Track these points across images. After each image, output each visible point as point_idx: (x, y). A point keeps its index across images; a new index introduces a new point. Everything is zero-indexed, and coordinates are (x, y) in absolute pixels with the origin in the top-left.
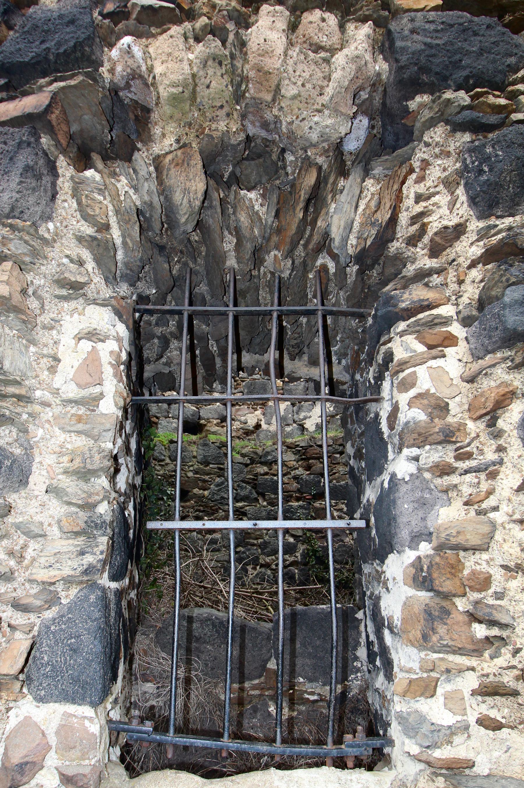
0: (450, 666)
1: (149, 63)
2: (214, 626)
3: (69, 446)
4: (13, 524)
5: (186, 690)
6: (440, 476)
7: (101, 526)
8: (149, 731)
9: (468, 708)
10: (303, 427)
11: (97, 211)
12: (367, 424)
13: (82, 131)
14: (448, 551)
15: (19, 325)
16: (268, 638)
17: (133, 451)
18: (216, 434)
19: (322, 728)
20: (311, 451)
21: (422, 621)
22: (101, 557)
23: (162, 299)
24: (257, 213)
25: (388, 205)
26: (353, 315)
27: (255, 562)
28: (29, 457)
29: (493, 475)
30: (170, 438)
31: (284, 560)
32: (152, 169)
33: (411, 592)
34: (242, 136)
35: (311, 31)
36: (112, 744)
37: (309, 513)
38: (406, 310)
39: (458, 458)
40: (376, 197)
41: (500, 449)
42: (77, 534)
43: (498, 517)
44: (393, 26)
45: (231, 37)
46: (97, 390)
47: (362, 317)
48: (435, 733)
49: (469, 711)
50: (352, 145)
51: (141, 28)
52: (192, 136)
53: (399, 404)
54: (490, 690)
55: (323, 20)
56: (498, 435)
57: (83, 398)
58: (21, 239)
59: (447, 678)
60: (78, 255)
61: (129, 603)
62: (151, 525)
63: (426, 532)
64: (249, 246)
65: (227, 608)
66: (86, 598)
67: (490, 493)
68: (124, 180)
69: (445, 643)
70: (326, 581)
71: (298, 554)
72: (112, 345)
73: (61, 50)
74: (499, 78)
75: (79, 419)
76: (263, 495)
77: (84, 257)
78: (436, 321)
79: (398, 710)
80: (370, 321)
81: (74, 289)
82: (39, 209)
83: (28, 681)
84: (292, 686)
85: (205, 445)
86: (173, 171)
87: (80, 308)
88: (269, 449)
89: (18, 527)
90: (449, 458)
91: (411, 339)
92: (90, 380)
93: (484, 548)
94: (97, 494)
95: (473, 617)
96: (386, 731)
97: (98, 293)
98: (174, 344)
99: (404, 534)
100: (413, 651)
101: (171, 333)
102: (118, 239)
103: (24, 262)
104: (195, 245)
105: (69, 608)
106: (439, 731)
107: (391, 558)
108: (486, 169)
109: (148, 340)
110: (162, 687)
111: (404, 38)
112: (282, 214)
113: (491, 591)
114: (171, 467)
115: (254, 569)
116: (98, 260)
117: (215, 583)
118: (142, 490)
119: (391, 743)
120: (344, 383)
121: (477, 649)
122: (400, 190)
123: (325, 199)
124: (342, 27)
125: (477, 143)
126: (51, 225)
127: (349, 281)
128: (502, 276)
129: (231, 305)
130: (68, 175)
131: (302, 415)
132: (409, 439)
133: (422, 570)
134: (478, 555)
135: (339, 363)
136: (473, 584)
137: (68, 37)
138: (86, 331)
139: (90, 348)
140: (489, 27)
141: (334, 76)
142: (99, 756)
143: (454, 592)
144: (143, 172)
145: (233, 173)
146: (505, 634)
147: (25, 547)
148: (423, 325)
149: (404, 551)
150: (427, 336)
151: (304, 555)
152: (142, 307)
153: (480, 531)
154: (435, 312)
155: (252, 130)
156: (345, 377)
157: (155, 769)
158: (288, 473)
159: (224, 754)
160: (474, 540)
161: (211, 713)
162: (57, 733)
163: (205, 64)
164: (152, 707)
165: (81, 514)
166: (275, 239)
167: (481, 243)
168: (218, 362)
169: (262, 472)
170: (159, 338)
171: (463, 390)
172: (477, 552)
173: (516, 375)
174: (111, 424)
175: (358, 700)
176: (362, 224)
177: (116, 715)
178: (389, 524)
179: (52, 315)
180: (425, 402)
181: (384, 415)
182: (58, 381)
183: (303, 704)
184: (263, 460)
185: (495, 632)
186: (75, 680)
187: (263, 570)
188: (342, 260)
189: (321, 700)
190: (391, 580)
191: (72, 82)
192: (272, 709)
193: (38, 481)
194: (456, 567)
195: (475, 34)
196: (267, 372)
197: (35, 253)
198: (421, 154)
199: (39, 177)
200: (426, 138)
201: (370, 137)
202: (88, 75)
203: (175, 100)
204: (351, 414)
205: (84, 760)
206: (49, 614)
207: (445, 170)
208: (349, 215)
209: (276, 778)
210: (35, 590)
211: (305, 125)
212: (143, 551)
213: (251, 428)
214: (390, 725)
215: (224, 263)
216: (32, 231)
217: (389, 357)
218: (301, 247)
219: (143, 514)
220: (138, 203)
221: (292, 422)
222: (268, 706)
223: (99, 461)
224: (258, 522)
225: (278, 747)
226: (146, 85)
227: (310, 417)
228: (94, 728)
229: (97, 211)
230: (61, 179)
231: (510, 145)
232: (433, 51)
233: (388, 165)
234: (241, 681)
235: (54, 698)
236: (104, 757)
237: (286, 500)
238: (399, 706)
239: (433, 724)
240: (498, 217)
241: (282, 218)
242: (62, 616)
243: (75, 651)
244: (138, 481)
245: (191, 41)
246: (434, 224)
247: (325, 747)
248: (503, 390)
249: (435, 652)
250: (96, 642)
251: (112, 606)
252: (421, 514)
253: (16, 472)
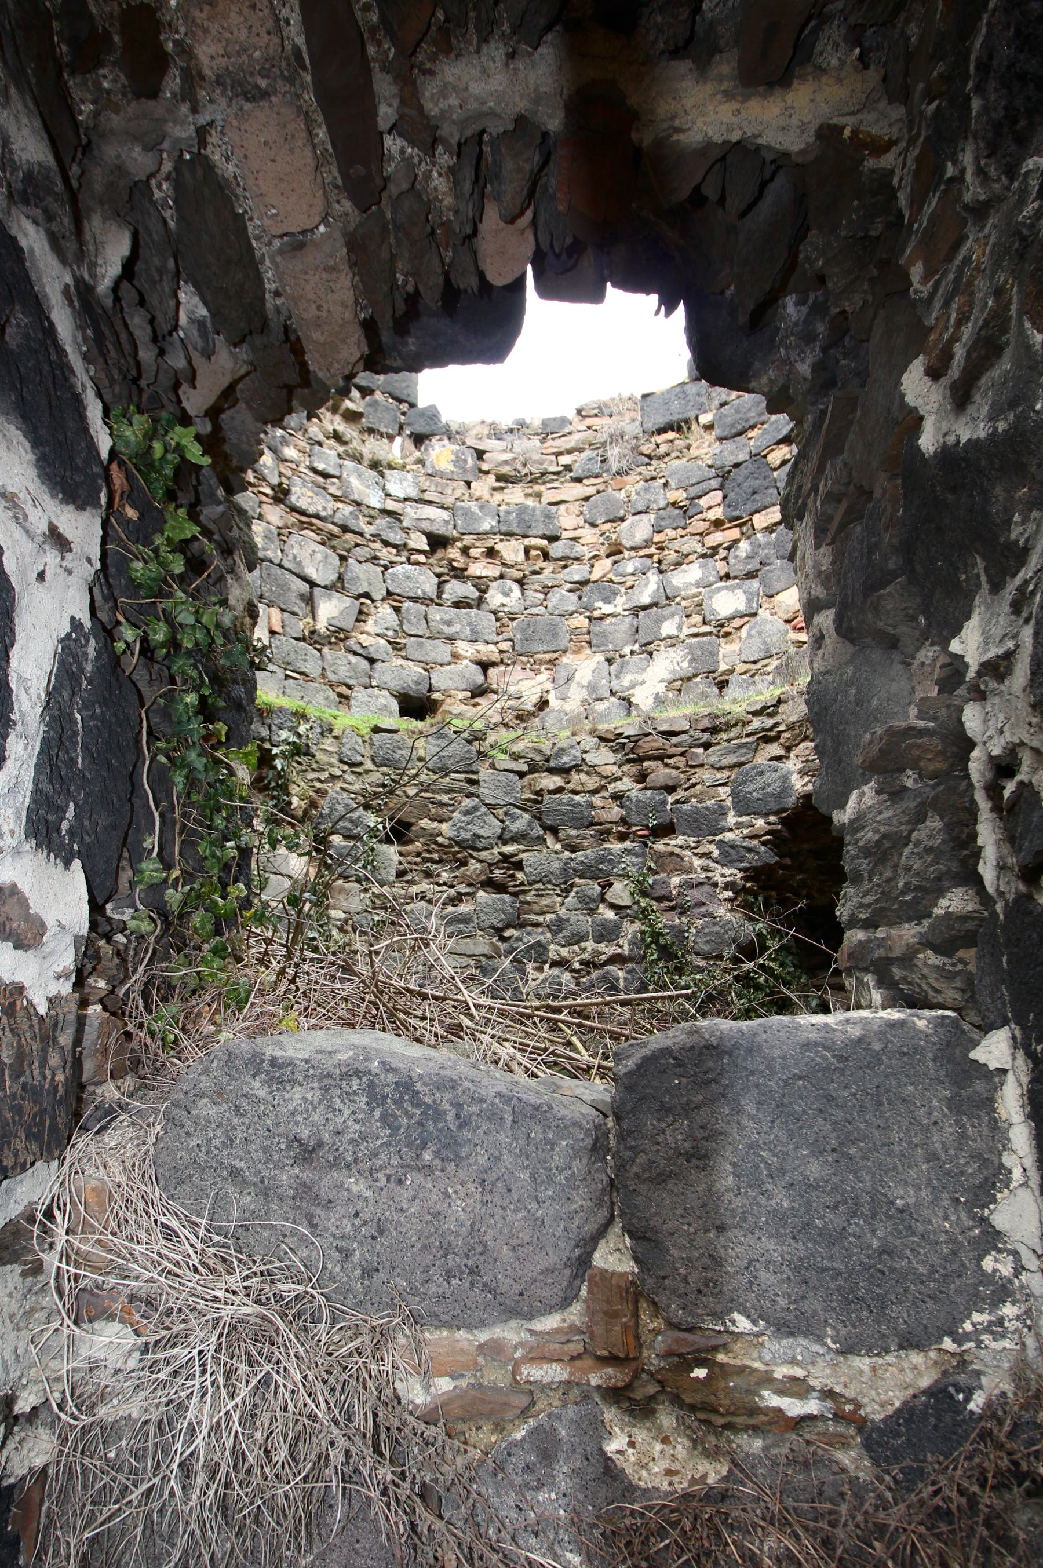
2: (375, 1097)
10: (630, 703)
30: (373, 723)
37: (644, 863)
76: (554, 831)
88: (564, 744)
115: (540, 969)
120: (881, 147)
131: (627, 680)
169: (552, 787)
184: (552, 764)
187: (556, 971)
213: (529, 707)
221: (607, 694)
227: (643, 683)
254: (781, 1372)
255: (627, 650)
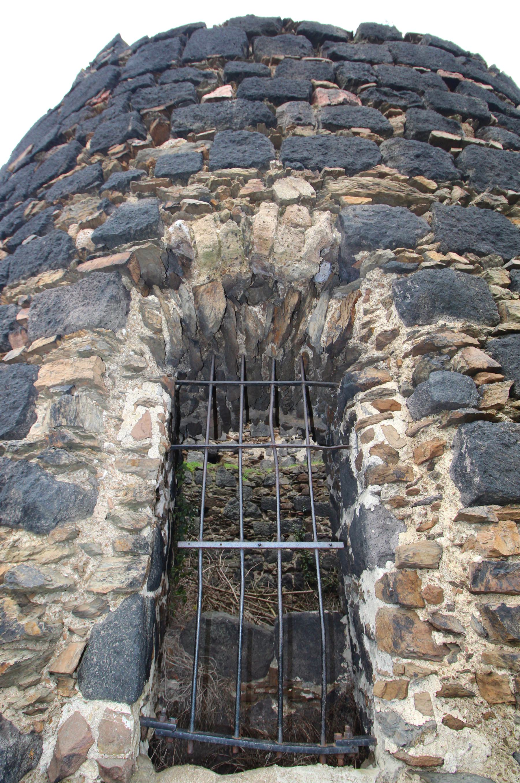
0: (417, 670)
1: (192, 234)
2: (227, 629)
3: (125, 484)
4: (79, 544)
5: (204, 687)
6: (398, 507)
7: (144, 547)
8: (173, 727)
9: (435, 709)
11: (155, 321)
12: (341, 464)
13: (148, 272)
14: (408, 570)
15: (97, 397)
16: (271, 640)
17: (170, 483)
18: (231, 462)
19: (316, 725)
20: (301, 477)
21: (392, 630)
22: (143, 572)
23: (194, 375)
24: (260, 320)
25: (346, 317)
26: (327, 386)
27: (260, 568)
28: (96, 490)
29: (436, 508)
30: (196, 466)
31: (283, 567)
32: (191, 294)
33: (382, 604)
34: (250, 275)
35: (292, 216)
36: (143, 738)
38: (364, 384)
39: (409, 494)
40: (338, 311)
41: (439, 488)
42: (126, 553)
43: (443, 541)
44: (343, 213)
45: (243, 221)
46: (147, 441)
47: (333, 387)
48: (409, 733)
49: (435, 712)
50: (321, 279)
51: (188, 215)
52: (218, 275)
53: (364, 452)
54: (451, 693)
55: (299, 210)
56: (436, 477)
57: (137, 448)
58: (104, 340)
59: (415, 681)
60: (141, 350)
61: (161, 607)
62: (181, 545)
63: (389, 552)
64: (254, 342)
65: (238, 610)
66: (130, 606)
67: (435, 522)
68: (173, 301)
69: (412, 649)
70: (314, 585)
71: (294, 562)
72: (159, 409)
73: (139, 228)
74: (411, 242)
75: (134, 463)
76: (266, 512)
77: (144, 350)
78: (385, 392)
79: (378, 710)
80: (339, 391)
81: (136, 372)
82: (117, 321)
83: (80, 679)
84: (290, 686)
85: (222, 471)
86: (205, 296)
87: (139, 384)
88: (269, 475)
89: (83, 547)
90: (403, 493)
91: (367, 405)
92: (143, 434)
93: (435, 567)
94: (143, 521)
95: (433, 627)
96: (369, 730)
97: (152, 373)
98: (202, 404)
99: (373, 554)
100: (387, 657)
101: (200, 397)
102: (167, 338)
103: (104, 356)
104: (218, 340)
105: (116, 616)
106: (412, 730)
107: (365, 574)
108: (409, 295)
109: (184, 402)
110: (184, 684)
111: (349, 220)
112: (276, 320)
113: (444, 604)
114: (196, 489)
115: (259, 574)
116: (153, 352)
117: (228, 587)
118: (174, 512)
119: (374, 741)
121: (437, 654)
122: (354, 307)
123: (304, 312)
124: (311, 213)
125: (401, 280)
126: (124, 331)
127: (323, 363)
128: (426, 364)
129: (242, 379)
130: (137, 299)
132: (372, 478)
133: (389, 585)
134: (431, 573)
135: (319, 416)
136: (429, 597)
137: (143, 221)
138: (142, 400)
139: (144, 412)
140: (402, 213)
141: (307, 241)
142: (132, 750)
143: (415, 604)
144: (186, 296)
145: (244, 296)
146: (459, 641)
147: (86, 564)
148: (376, 395)
149: (374, 568)
150: (379, 403)
151: (299, 563)
152: (181, 381)
153: (431, 553)
154: (383, 386)
155: (255, 271)
156: (324, 427)
157: (177, 763)
158: (284, 494)
159: (235, 751)
160: (427, 561)
161: (224, 709)
162: (100, 728)
163: (227, 235)
164: (176, 703)
165: (130, 537)
166: (272, 336)
167: (410, 342)
168: (233, 416)
170: (191, 400)
171: (408, 443)
172: (430, 571)
173: (444, 433)
174: (155, 466)
175: (346, 699)
176: (329, 328)
177: (147, 711)
178: (362, 545)
179: (120, 389)
180: (382, 451)
181: (353, 459)
182: (121, 435)
183: (301, 702)
185: (451, 639)
186: (117, 680)
187: (266, 575)
188: (317, 350)
189: (316, 698)
190: (366, 593)
191: (144, 246)
192: (274, 706)
193: (101, 510)
194: (416, 583)
195: (394, 217)
196: (267, 423)
197: (113, 349)
198: (365, 286)
199: (119, 302)
200: (368, 276)
201: (332, 274)
202: (153, 242)
203: (207, 255)
204: (329, 455)
205: (120, 753)
206: (100, 620)
207: (382, 295)
208: (321, 322)
209: (278, 775)
210: (90, 599)
211: (290, 269)
212: (173, 562)
213: (256, 458)
214: (372, 724)
215: (238, 351)
216: (112, 335)
217: (353, 417)
218: (289, 341)
219: (177, 533)
220: (182, 315)
222: (271, 703)
223: (146, 495)
224: (262, 543)
225: (280, 744)
226: (190, 247)
228: (129, 724)
229: (155, 321)
230: (133, 302)
231: (423, 281)
232: (368, 227)
233: (344, 291)
234: (249, 681)
235: (100, 696)
236: (135, 751)
237: (284, 515)
238: (378, 707)
239: (407, 724)
240: (419, 325)
241: (276, 323)
242: (110, 622)
243: (118, 653)
244: (172, 505)
245: (218, 222)
246: (378, 328)
247: (319, 745)
248: (436, 444)
249: (404, 657)
250: (135, 646)
251: (149, 613)
252: (385, 538)
253: (86, 504)
254: (306, 689)
255: (294, 437)
